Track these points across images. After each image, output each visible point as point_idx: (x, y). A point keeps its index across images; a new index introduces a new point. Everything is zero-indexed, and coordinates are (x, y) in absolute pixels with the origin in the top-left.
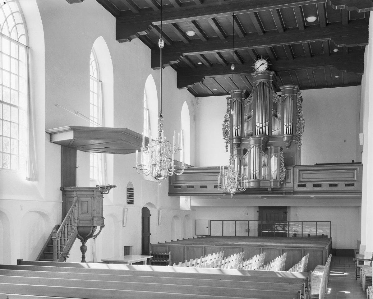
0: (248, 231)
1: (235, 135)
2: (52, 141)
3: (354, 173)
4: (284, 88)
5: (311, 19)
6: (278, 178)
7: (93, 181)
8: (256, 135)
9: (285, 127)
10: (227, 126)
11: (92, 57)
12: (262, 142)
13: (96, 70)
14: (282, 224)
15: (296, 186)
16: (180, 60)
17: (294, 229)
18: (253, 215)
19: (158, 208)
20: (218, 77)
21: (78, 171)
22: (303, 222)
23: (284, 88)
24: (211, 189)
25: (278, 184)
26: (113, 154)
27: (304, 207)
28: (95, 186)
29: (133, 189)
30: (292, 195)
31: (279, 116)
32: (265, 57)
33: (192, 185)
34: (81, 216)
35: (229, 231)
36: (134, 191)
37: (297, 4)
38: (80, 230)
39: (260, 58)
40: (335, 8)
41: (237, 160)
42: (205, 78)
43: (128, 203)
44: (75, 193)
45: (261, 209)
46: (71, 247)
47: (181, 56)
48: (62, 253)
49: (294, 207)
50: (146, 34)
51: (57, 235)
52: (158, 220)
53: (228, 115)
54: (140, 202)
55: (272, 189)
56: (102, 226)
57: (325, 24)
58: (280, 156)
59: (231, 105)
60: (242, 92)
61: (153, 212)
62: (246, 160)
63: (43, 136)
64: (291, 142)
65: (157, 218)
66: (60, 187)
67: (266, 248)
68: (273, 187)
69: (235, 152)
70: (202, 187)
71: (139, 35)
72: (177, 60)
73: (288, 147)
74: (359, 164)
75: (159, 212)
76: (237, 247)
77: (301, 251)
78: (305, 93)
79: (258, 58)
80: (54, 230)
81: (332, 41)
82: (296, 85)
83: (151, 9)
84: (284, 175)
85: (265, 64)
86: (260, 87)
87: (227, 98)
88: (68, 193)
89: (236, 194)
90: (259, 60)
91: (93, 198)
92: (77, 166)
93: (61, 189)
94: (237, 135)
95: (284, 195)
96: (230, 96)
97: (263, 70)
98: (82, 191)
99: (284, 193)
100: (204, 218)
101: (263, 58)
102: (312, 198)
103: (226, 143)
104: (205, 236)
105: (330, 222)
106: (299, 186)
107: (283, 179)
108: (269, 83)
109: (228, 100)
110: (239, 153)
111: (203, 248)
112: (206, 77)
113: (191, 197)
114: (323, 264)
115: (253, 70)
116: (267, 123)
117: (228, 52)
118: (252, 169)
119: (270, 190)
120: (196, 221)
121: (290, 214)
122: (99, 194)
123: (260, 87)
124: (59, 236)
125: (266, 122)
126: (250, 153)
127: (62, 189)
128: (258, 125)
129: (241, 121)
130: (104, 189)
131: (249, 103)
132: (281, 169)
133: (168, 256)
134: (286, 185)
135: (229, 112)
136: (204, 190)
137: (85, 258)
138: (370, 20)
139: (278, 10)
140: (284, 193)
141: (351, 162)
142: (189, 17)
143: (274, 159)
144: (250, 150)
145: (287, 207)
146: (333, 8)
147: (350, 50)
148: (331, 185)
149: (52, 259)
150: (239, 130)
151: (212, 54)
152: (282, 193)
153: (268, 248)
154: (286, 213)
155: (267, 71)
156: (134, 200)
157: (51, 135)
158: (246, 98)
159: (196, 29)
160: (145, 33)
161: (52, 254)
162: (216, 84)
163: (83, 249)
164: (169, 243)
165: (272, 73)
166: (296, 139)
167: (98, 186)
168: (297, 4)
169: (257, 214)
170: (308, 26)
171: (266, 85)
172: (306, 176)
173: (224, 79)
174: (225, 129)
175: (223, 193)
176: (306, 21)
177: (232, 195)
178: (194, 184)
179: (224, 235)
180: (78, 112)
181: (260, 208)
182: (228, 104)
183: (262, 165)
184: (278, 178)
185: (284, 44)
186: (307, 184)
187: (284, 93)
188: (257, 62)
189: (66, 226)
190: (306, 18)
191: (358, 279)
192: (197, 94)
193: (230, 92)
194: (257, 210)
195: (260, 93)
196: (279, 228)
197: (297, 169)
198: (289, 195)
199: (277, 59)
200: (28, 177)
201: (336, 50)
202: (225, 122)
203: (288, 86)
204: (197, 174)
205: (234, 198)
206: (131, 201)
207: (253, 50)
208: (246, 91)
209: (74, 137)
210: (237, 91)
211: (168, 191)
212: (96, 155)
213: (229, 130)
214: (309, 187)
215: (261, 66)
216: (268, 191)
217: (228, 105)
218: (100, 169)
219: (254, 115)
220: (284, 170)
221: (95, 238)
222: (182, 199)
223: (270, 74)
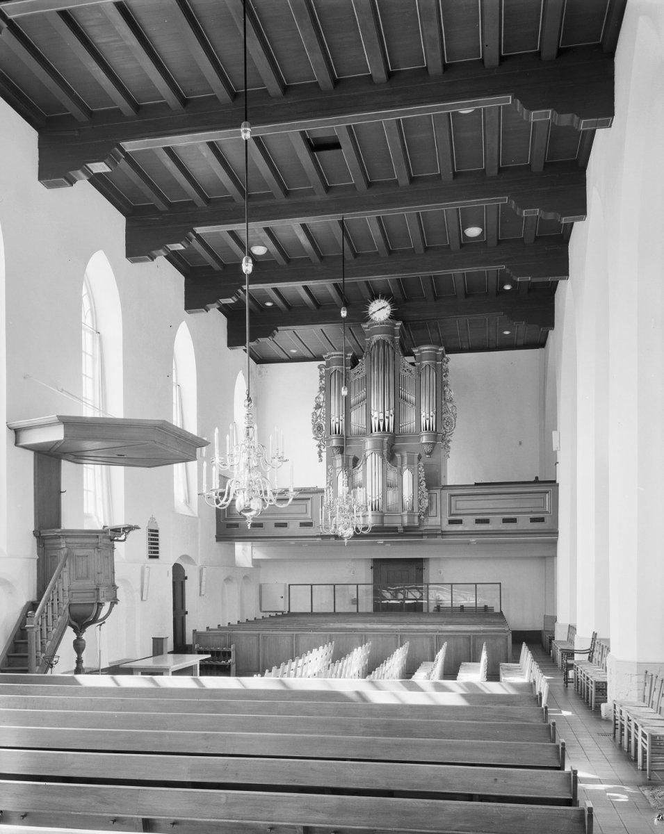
0: (356, 602)
1: (336, 433)
2: (20, 444)
3: (544, 499)
5: (473, 232)
6: (416, 509)
7: (88, 516)
8: (372, 432)
9: (423, 420)
10: (320, 416)
11: (84, 291)
12: (385, 445)
13: (90, 312)
14: (392, 590)
15: (445, 522)
16: (237, 297)
17: (439, 596)
18: (364, 574)
19: (199, 564)
20: (301, 330)
21: (64, 498)
22: (453, 586)
23: (420, 351)
25: (416, 518)
26: (448, 484)
28: (100, 528)
29: (157, 531)
30: (439, 539)
31: (413, 398)
32: (386, 296)
33: (512, 516)
34: (75, 584)
35: (323, 603)
36: (160, 533)
37: (452, 205)
38: (74, 609)
39: (377, 298)
40: (521, 213)
41: (342, 478)
42: (278, 331)
43: (150, 557)
44: (62, 540)
45: (378, 564)
46: (59, 643)
47: (240, 291)
48: (44, 655)
49: (436, 559)
50: (182, 248)
51: (35, 622)
52: (200, 585)
53: (322, 396)
54: (170, 553)
55: (404, 527)
56: (114, 601)
57: (458, 245)
58: (418, 471)
59: (327, 377)
60: (437, 351)
61: (190, 571)
62: (359, 477)
64: (434, 445)
65: (199, 582)
66: (33, 530)
67: (406, 634)
68: (406, 525)
69: (339, 463)
70: (277, 525)
71: (169, 250)
72: (234, 298)
73: (429, 454)
74: (551, 484)
75: (201, 571)
77: (469, 638)
79: (375, 297)
80: (30, 612)
81: (508, 271)
82: (441, 346)
83: (192, 204)
84: (426, 503)
85: (386, 309)
86: (379, 348)
87: (320, 367)
88: (47, 542)
90: (377, 301)
91: (96, 550)
93: (35, 533)
94: (338, 432)
95: (425, 539)
96: (324, 363)
97: (382, 319)
99: (425, 535)
100: (277, 581)
101: (382, 298)
103: (319, 446)
104: (281, 614)
105: (500, 584)
106: (451, 522)
107: (424, 511)
109: (321, 370)
110: (345, 466)
111: (292, 637)
112: (279, 328)
113: (252, 544)
114: (476, 659)
115: (366, 318)
116: (392, 411)
117: (324, 286)
119: (400, 530)
120: (261, 586)
122: (107, 541)
123: (379, 348)
124: (38, 624)
125: (389, 410)
126: (366, 464)
127: (38, 534)
128: (375, 414)
129: (435, 406)
130: (114, 534)
131: (360, 376)
132: (420, 492)
133: (229, 653)
134: (427, 521)
135: (323, 392)
136: (282, 531)
137: (82, 662)
139: (379, 217)
140: (425, 535)
141: (533, 479)
142: (261, 220)
143: (407, 475)
144: (366, 460)
145: (422, 559)
146: (518, 213)
147: (532, 287)
148: (505, 521)
149: (27, 665)
150: (342, 424)
151: (294, 288)
152: (421, 536)
153: (412, 634)
154: (422, 569)
155: (391, 321)
156: (160, 550)
157: (17, 432)
158: (352, 368)
159: (270, 242)
160: (179, 247)
161: (27, 657)
162: (296, 342)
163: (79, 646)
164: (224, 628)
165: (399, 324)
166: (443, 440)
167: (106, 528)
168: (452, 205)
169: (370, 572)
170: (467, 243)
171: (388, 345)
172: (463, 505)
173: (312, 334)
174: (317, 420)
175: (317, 536)
176: (464, 234)
177: (346, 541)
179: (314, 611)
181: (375, 561)
182: (320, 376)
183: (387, 485)
184: (416, 509)
185: (420, 274)
187: (420, 359)
188: (373, 304)
189: (50, 604)
190: (464, 229)
191: (569, 684)
192: (261, 359)
193: (324, 356)
194: (370, 564)
195: (378, 358)
196: (388, 595)
197: (447, 493)
198: (433, 539)
199: (406, 300)
201: (508, 287)
202: (316, 408)
203: (426, 348)
205: (349, 544)
206: (154, 554)
207: (367, 282)
208: (354, 354)
209: (65, 436)
210: (337, 355)
211: (214, 533)
212: (91, 469)
213: (323, 424)
214: (469, 524)
215: (380, 311)
216: (397, 531)
217: (321, 379)
218: (99, 496)
219: (367, 398)
220: (426, 494)
221: (101, 625)
222: (239, 546)
223: (396, 326)
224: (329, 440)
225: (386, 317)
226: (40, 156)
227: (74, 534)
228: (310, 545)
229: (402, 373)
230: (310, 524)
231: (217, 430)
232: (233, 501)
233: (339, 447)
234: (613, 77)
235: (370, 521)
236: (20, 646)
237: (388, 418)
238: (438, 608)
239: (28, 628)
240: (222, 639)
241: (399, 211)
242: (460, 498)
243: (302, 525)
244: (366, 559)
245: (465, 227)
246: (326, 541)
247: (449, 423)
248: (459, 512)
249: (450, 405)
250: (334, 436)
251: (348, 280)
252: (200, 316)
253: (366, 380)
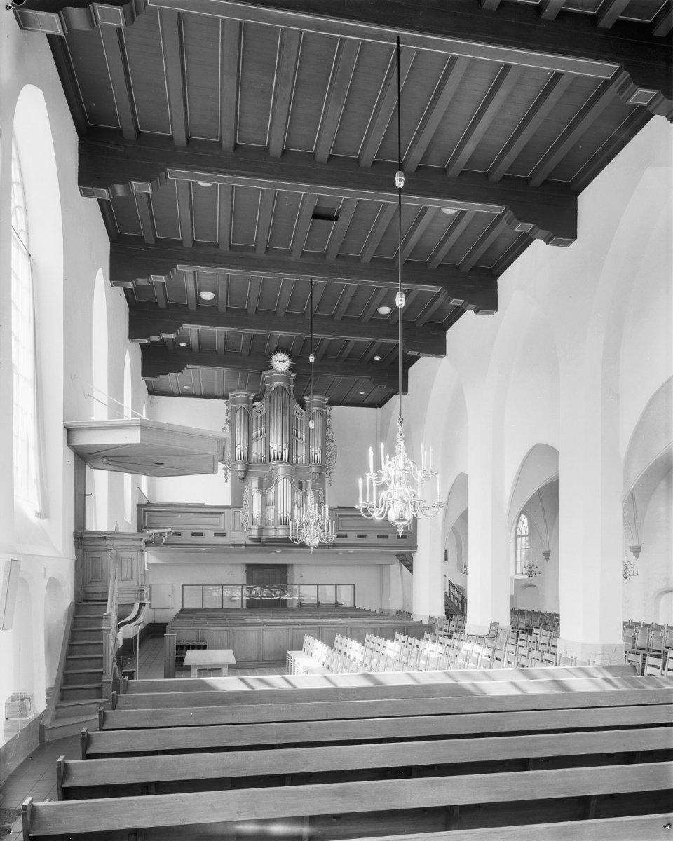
4: (309, 400)
8: (270, 461)
18: (240, 576)
23: (309, 400)
27: (313, 565)
32: (285, 351)
33: (384, 533)
49: (300, 565)
62: (271, 497)
78: (336, 411)
89: (321, 545)
92: (87, 494)
94: (316, 461)
97: (283, 370)
103: (225, 469)
106: (339, 536)
108: (289, 389)
115: (270, 367)
121: (292, 575)
131: (259, 414)
136: (177, 539)
145: (286, 565)
148: (359, 537)
157: (69, 431)
165: (294, 375)
175: (232, 545)
177: (312, 549)
178: (182, 529)
179: (224, 607)
181: (248, 566)
194: (245, 569)
200: (38, 511)
205: (314, 553)
209: (141, 439)
215: (281, 363)
224: (234, 465)
225: (286, 368)
226: (79, 162)
229: (295, 415)
230: (223, 535)
231: (371, 450)
233: (244, 471)
234: (576, 210)
235: (255, 534)
236: (75, 648)
237: (243, 451)
238: (300, 604)
239: (104, 630)
240: (195, 633)
241: (341, 281)
243: (216, 535)
249: (332, 445)
251: (315, 336)
253: (266, 418)
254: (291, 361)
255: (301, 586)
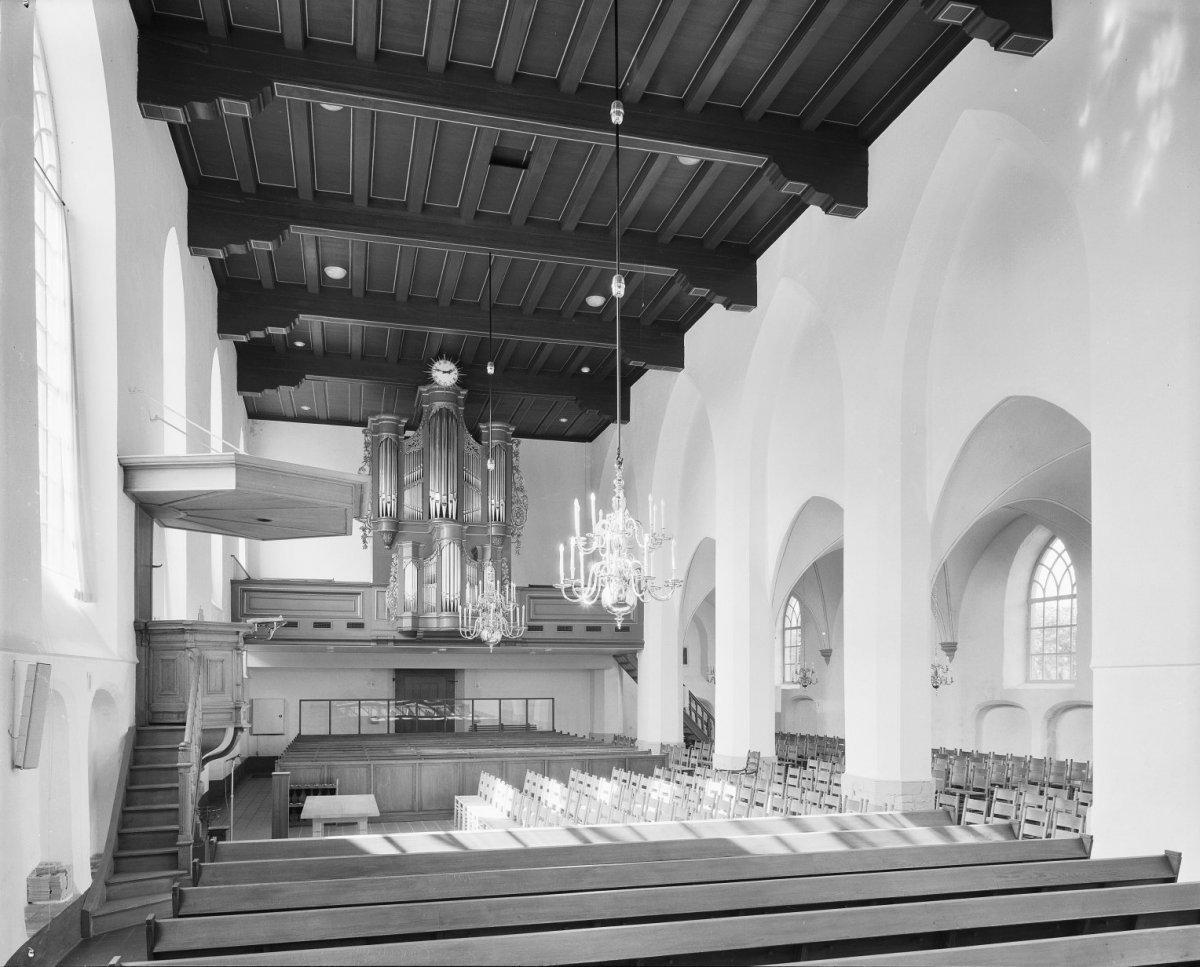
4: (488, 428)
18: (386, 687)
24: (339, 629)
49: (476, 670)
60: (400, 423)
63: (113, 476)
70: (317, 625)
76: (496, 759)
78: (527, 447)
79: (439, 357)
89: (505, 641)
91: (235, 652)
92: (154, 564)
98: (210, 632)
102: (544, 653)
105: (301, 701)
106: (531, 628)
112: (307, 376)
115: (428, 380)
118: (445, 590)
136: (292, 633)
138: (216, 321)
165: (465, 392)
169: (392, 684)
175: (373, 641)
177: (491, 647)
180: (156, 416)
181: (398, 671)
182: (365, 443)
186: (334, 623)
194: (392, 675)
200: (79, 590)
204: (322, 597)
209: (237, 485)
210: (390, 420)
215: (445, 374)
224: (376, 524)
225: (454, 382)
227: (211, 628)
228: (336, 651)
230: (360, 626)
231: (576, 502)
232: (599, 599)
235: (407, 624)
238: (475, 727)
240: (318, 772)
242: (539, 601)
244: (390, 669)
245: (591, 293)
246: (382, 646)
247: (519, 514)
248: (539, 617)
250: (383, 519)
251: (496, 335)
252: (225, 342)
253: (423, 456)
254: (460, 372)
255: (529, 701)
